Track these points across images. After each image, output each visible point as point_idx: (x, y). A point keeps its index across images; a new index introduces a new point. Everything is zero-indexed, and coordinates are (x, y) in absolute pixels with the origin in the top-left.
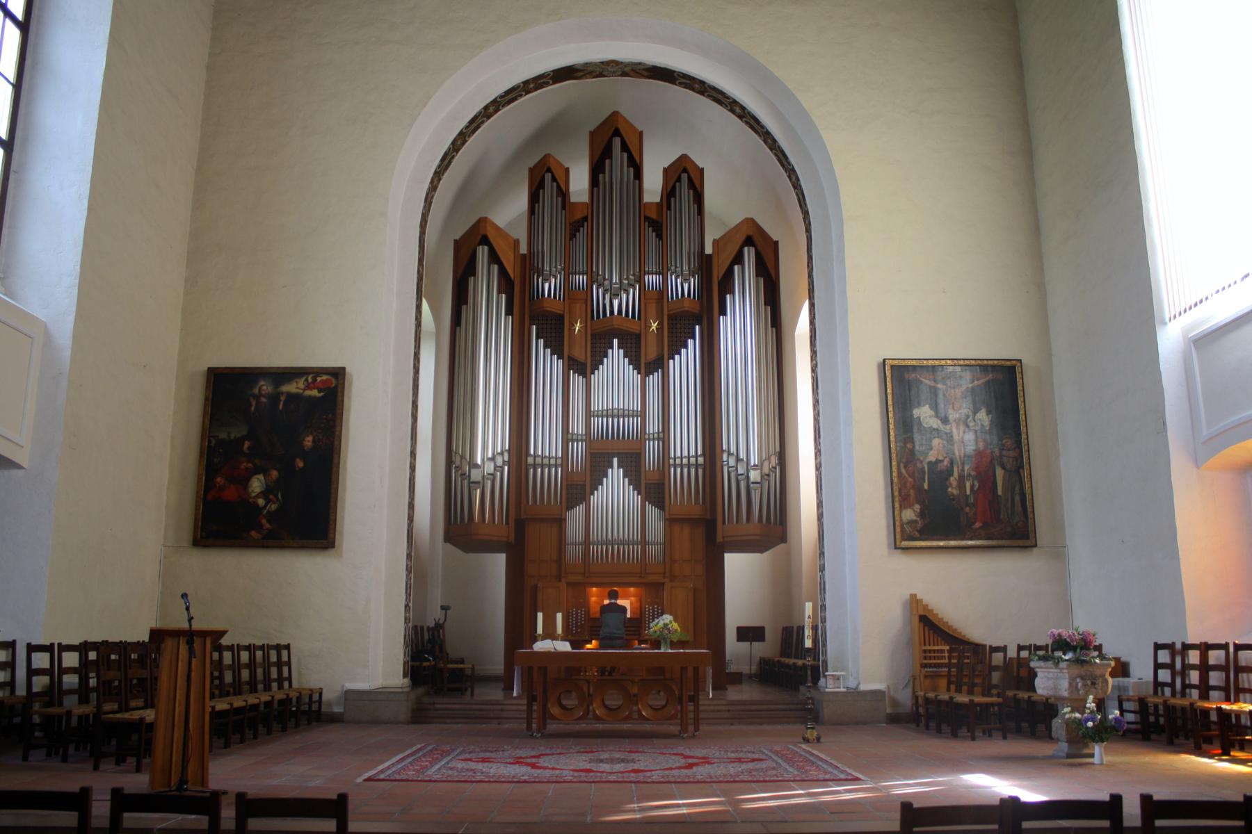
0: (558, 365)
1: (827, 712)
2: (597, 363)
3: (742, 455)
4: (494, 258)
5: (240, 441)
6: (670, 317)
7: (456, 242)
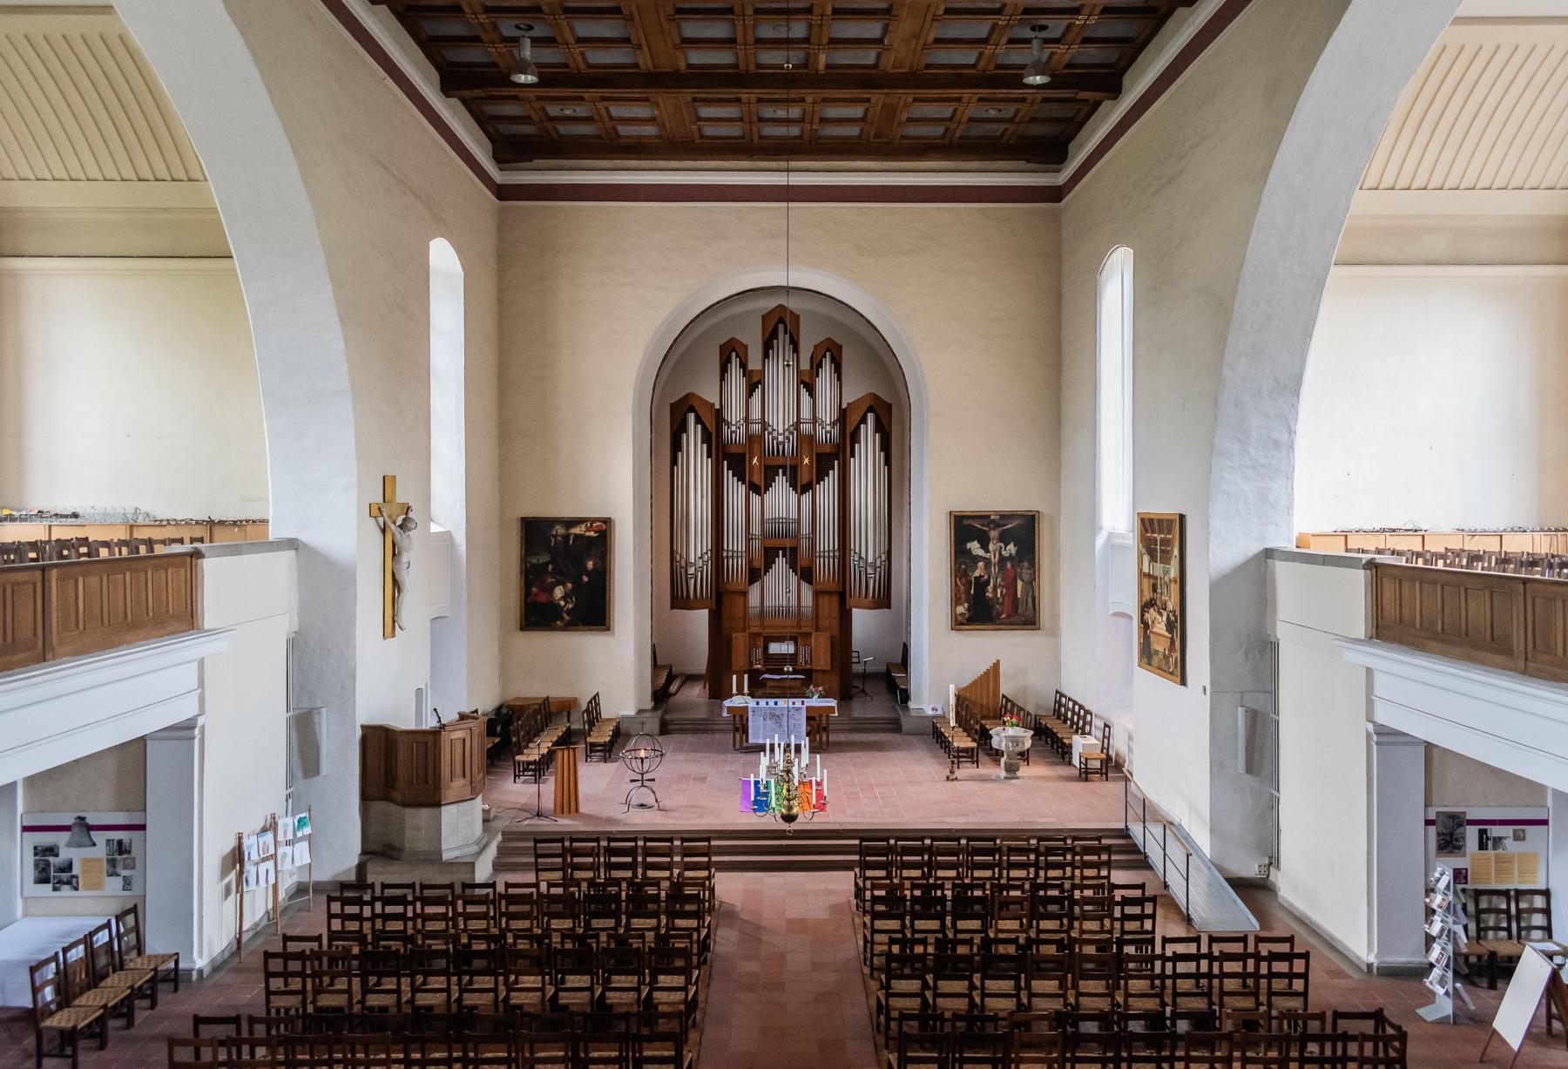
0: (742, 489)
1: (905, 727)
2: (768, 486)
3: (863, 555)
4: (698, 420)
5: (547, 564)
6: (818, 455)
7: (672, 406)
